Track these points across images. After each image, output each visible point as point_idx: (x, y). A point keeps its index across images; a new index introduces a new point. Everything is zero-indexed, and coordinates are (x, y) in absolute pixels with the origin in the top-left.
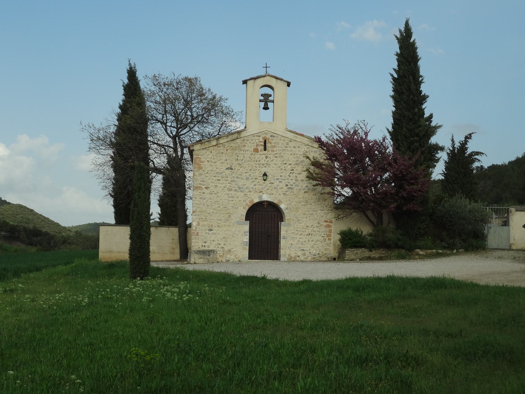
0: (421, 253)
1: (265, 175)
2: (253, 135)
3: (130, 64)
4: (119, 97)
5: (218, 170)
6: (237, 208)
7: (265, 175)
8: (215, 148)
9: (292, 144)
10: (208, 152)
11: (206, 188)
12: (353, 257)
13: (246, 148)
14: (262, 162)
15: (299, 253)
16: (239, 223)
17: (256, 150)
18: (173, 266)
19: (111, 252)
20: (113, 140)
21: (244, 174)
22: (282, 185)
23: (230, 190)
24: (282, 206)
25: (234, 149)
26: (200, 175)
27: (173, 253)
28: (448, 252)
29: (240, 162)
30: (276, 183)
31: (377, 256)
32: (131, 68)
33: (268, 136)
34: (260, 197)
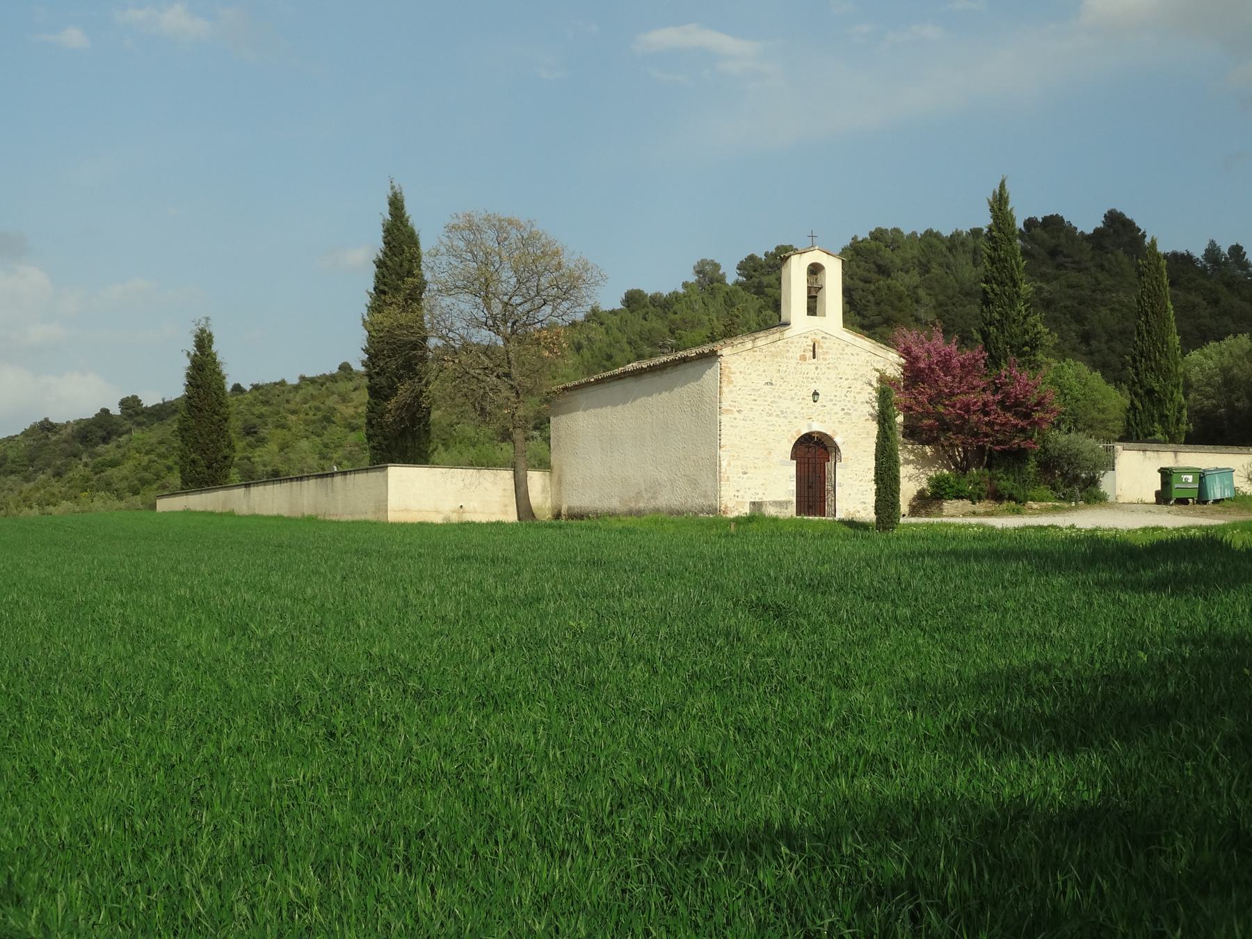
0: (1035, 506)
1: (816, 394)
2: (800, 336)
3: (393, 188)
4: (375, 244)
5: (753, 386)
6: (779, 442)
7: (816, 394)
8: (751, 353)
9: (849, 350)
10: (741, 359)
11: (739, 411)
12: (952, 512)
13: (790, 354)
14: (811, 375)
15: (860, 507)
16: (783, 463)
17: (803, 358)
18: (974, 520)
19: (407, 510)
20: (367, 318)
21: (788, 393)
22: (837, 409)
23: (770, 415)
24: (838, 440)
25: (774, 355)
26: (731, 391)
27: (506, 513)
28: (1066, 505)
29: (782, 374)
30: (829, 405)
31: (982, 510)
32: (395, 195)
33: (818, 338)
34: (810, 426)
